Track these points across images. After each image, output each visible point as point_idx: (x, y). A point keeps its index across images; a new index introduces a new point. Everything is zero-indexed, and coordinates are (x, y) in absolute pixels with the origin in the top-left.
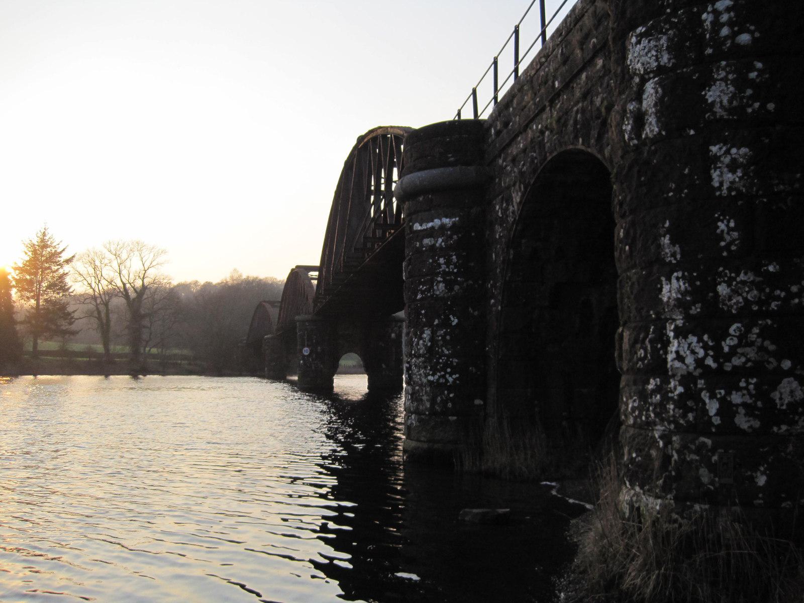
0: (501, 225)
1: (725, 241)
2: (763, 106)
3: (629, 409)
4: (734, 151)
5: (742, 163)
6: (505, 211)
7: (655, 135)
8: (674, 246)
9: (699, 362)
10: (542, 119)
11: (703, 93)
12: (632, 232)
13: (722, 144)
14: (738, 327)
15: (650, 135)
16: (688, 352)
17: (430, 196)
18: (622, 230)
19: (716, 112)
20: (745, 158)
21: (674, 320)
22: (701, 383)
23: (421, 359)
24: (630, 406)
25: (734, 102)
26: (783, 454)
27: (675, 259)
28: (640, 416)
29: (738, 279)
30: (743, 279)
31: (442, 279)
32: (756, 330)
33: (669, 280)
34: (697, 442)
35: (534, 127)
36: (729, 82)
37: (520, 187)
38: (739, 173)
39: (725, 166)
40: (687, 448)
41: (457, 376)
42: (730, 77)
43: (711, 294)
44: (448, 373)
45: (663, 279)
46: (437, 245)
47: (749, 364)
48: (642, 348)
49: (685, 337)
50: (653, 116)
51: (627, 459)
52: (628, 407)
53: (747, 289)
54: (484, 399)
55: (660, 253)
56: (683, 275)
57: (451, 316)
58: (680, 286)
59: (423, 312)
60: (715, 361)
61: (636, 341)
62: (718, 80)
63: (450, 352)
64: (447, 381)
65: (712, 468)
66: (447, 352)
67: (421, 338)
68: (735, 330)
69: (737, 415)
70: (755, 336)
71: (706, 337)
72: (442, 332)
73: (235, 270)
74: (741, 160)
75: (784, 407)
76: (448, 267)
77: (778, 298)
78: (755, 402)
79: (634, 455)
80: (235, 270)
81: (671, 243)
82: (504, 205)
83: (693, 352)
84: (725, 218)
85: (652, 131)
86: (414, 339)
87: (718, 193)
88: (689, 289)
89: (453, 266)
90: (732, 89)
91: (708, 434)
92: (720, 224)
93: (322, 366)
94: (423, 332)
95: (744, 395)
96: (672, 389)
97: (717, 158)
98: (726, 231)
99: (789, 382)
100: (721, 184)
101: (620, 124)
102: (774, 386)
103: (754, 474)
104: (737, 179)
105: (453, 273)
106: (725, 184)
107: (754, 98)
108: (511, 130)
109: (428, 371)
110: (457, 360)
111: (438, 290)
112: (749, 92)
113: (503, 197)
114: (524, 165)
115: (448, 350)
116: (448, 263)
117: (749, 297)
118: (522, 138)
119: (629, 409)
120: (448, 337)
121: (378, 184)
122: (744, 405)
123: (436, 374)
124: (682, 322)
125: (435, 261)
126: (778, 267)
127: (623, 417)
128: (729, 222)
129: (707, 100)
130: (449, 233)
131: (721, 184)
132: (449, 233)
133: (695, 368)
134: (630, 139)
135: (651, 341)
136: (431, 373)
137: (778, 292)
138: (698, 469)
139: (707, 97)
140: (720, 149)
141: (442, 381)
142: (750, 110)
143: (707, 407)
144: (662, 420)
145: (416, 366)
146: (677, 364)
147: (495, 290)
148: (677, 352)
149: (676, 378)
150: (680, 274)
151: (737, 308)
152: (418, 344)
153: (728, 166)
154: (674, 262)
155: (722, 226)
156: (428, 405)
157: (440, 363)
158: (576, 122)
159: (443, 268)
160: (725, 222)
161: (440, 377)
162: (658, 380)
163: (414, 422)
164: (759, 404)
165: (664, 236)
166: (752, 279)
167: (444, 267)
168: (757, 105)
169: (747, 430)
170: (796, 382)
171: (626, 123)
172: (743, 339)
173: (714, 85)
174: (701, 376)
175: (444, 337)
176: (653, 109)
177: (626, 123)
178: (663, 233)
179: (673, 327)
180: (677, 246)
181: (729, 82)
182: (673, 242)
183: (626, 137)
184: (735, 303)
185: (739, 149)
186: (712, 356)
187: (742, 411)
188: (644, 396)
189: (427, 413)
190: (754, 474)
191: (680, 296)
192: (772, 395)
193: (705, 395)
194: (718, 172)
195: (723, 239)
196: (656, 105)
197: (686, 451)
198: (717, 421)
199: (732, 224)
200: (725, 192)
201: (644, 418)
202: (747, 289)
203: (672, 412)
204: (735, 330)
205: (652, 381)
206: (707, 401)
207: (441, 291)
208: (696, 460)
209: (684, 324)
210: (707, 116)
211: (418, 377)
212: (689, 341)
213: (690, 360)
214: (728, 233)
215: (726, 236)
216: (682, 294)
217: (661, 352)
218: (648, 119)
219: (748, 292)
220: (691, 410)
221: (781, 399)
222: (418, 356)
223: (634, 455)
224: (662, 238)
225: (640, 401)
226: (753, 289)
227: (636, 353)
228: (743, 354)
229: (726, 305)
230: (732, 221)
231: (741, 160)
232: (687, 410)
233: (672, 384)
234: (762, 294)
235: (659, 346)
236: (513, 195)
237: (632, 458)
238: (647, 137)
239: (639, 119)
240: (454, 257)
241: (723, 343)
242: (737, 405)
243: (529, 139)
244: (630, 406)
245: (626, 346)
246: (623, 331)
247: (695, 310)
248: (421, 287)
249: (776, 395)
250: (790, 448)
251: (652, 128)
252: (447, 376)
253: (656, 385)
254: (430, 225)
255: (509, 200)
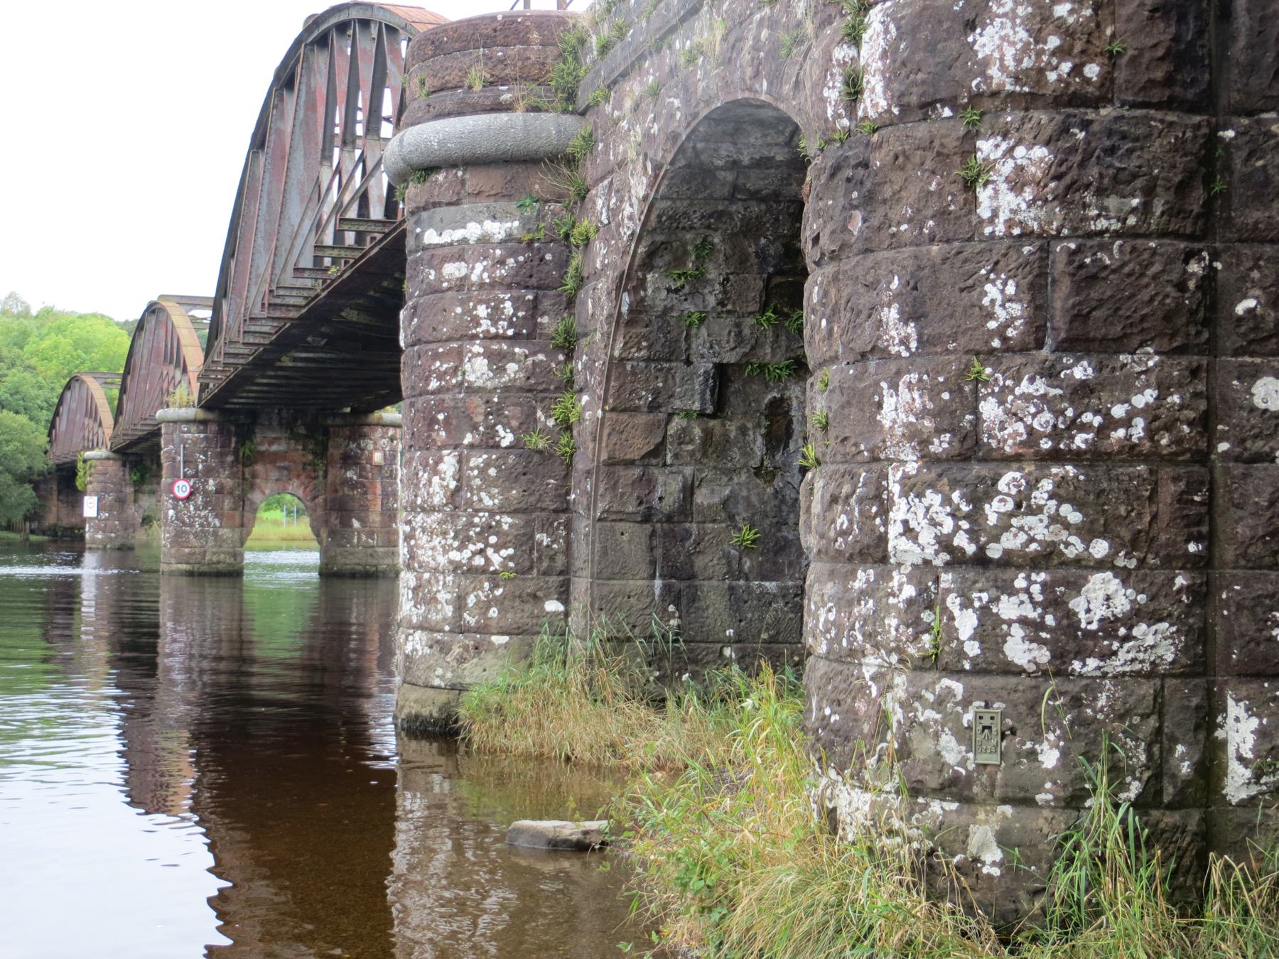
0: (606, 241)
1: (997, 319)
2: (1077, 70)
3: (821, 626)
4: (1020, 151)
5: (1034, 175)
6: (614, 212)
7: (880, 114)
8: (906, 324)
9: (945, 544)
10: (692, 29)
11: (970, 39)
12: (833, 292)
13: (999, 138)
14: (1014, 479)
15: (872, 113)
16: (924, 522)
17: (460, 173)
18: (816, 288)
19: (992, 78)
20: (1039, 167)
21: (903, 462)
22: (947, 579)
23: (437, 516)
24: (822, 619)
25: (1026, 59)
26: (1089, 711)
27: (908, 349)
28: (838, 639)
29: (1018, 391)
30: (1026, 391)
31: (481, 350)
32: (1047, 485)
33: (894, 386)
34: (938, 688)
35: (678, 45)
36: (1018, 21)
37: (645, 168)
38: (1028, 194)
39: (1003, 178)
40: (919, 698)
41: (511, 551)
42: (1021, 11)
43: (968, 417)
44: (492, 546)
45: (884, 385)
46: (474, 278)
47: (1034, 546)
48: (846, 513)
49: (920, 495)
50: (878, 77)
51: (817, 719)
52: (818, 620)
53: (1032, 410)
54: (565, 600)
55: (879, 338)
56: (920, 380)
57: (499, 428)
58: (913, 400)
59: (441, 417)
60: (971, 540)
61: (834, 500)
62: (999, 16)
63: (496, 501)
64: (488, 560)
65: (964, 734)
66: (491, 503)
67: (435, 472)
68: (1008, 485)
69: (1009, 638)
70: (1046, 495)
71: (956, 496)
72: (480, 460)
73: (12, 296)
74: (1033, 169)
75: (1094, 627)
76: (495, 324)
77: (1085, 428)
78: (1042, 617)
79: (827, 711)
80: (12, 296)
81: (900, 320)
82: (614, 200)
83: (934, 523)
84: (998, 277)
85: (875, 105)
86: (421, 474)
87: (987, 230)
88: (930, 406)
89: (506, 323)
90: (1022, 34)
91: (957, 673)
92: (988, 287)
93: (217, 523)
94: (439, 460)
95: (1022, 602)
96: (896, 589)
97: (990, 165)
98: (999, 302)
99: (1104, 582)
100: (995, 214)
101: (821, 83)
102: (1076, 586)
103: (1037, 747)
104: (1024, 206)
105: (504, 338)
106: (1001, 214)
107: (1061, 53)
108: (630, 43)
109: (450, 541)
110: (510, 520)
111: (474, 372)
112: (1054, 42)
113: (611, 183)
114: (654, 120)
115: (492, 497)
116: (494, 317)
117: (1036, 426)
118: (652, 65)
119: (821, 626)
120: (492, 472)
121: (349, 122)
122: (1023, 621)
123: (466, 547)
124: (916, 466)
125: (469, 312)
126: (1090, 371)
127: (810, 640)
128: (1005, 284)
129: (976, 53)
130: (498, 252)
131: (995, 214)
132: (498, 252)
133: (937, 553)
134: (837, 116)
135: (861, 501)
136: (456, 544)
137: (1087, 417)
138: (937, 736)
139: (976, 47)
140: (997, 146)
141: (479, 561)
142: (1052, 76)
143: (957, 624)
144: (877, 646)
145: (424, 530)
146: (904, 544)
147: (591, 374)
148: (905, 523)
149: (902, 569)
150: (914, 377)
151: (1014, 444)
152: (430, 482)
153: (1007, 180)
154: (905, 354)
155: (992, 291)
156: (449, 611)
157: (476, 525)
158: (756, 48)
159: (483, 328)
160: (999, 282)
161: (474, 554)
162: (871, 572)
163: (419, 647)
164: (1050, 620)
165: (889, 306)
166: (1042, 391)
167: (485, 324)
168: (1066, 67)
169: (1026, 667)
170: (1117, 581)
171: (831, 84)
172: (1022, 505)
173: (992, 24)
174: (948, 565)
175: (483, 471)
176: (880, 64)
177: (831, 84)
178: (886, 299)
179: (899, 474)
180: (912, 325)
181: (1018, 21)
182: (905, 318)
183: (830, 112)
184: (1009, 435)
185: (1029, 148)
186: (966, 531)
187: (1017, 631)
188: (846, 602)
189: (447, 628)
190: (1037, 747)
191: (912, 419)
192: (1072, 604)
193: (953, 602)
194: (989, 190)
195: (991, 316)
196: (884, 55)
197: (917, 704)
198: (973, 649)
199: (1011, 289)
200: (1000, 229)
201: (844, 643)
202: (1032, 410)
203: (893, 633)
204: (1008, 485)
205: (860, 574)
206: (956, 611)
207: (479, 374)
208: (936, 721)
209: (919, 470)
210: (974, 83)
211: (430, 553)
212: (926, 501)
213: (927, 536)
214: (1003, 306)
215: (998, 310)
216: (916, 415)
217: (878, 521)
218: (868, 82)
219: (1034, 416)
220: (928, 629)
221: (1088, 611)
222: (429, 510)
223: (827, 711)
224: (886, 309)
225: (838, 612)
226: (1043, 410)
227: (833, 521)
228: (1021, 528)
229: (994, 437)
230: (1010, 282)
231: (1033, 169)
232: (920, 628)
233: (895, 583)
234: (1061, 419)
235: (874, 509)
236: (632, 182)
237: (824, 718)
238: (865, 118)
239: (854, 89)
240: (508, 304)
241: (987, 507)
242: (1010, 623)
243: (667, 69)
244: (822, 619)
245: (816, 508)
246: (813, 478)
247: (940, 445)
248: (438, 364)
249: (1077, 604)
250: (1102, 701)
251: (875, 100)
252: (490, 551)
253: (867, 581)
254: (458, 234)
255: (622, 192)
